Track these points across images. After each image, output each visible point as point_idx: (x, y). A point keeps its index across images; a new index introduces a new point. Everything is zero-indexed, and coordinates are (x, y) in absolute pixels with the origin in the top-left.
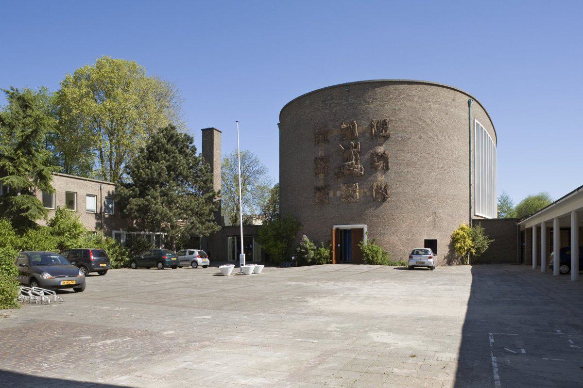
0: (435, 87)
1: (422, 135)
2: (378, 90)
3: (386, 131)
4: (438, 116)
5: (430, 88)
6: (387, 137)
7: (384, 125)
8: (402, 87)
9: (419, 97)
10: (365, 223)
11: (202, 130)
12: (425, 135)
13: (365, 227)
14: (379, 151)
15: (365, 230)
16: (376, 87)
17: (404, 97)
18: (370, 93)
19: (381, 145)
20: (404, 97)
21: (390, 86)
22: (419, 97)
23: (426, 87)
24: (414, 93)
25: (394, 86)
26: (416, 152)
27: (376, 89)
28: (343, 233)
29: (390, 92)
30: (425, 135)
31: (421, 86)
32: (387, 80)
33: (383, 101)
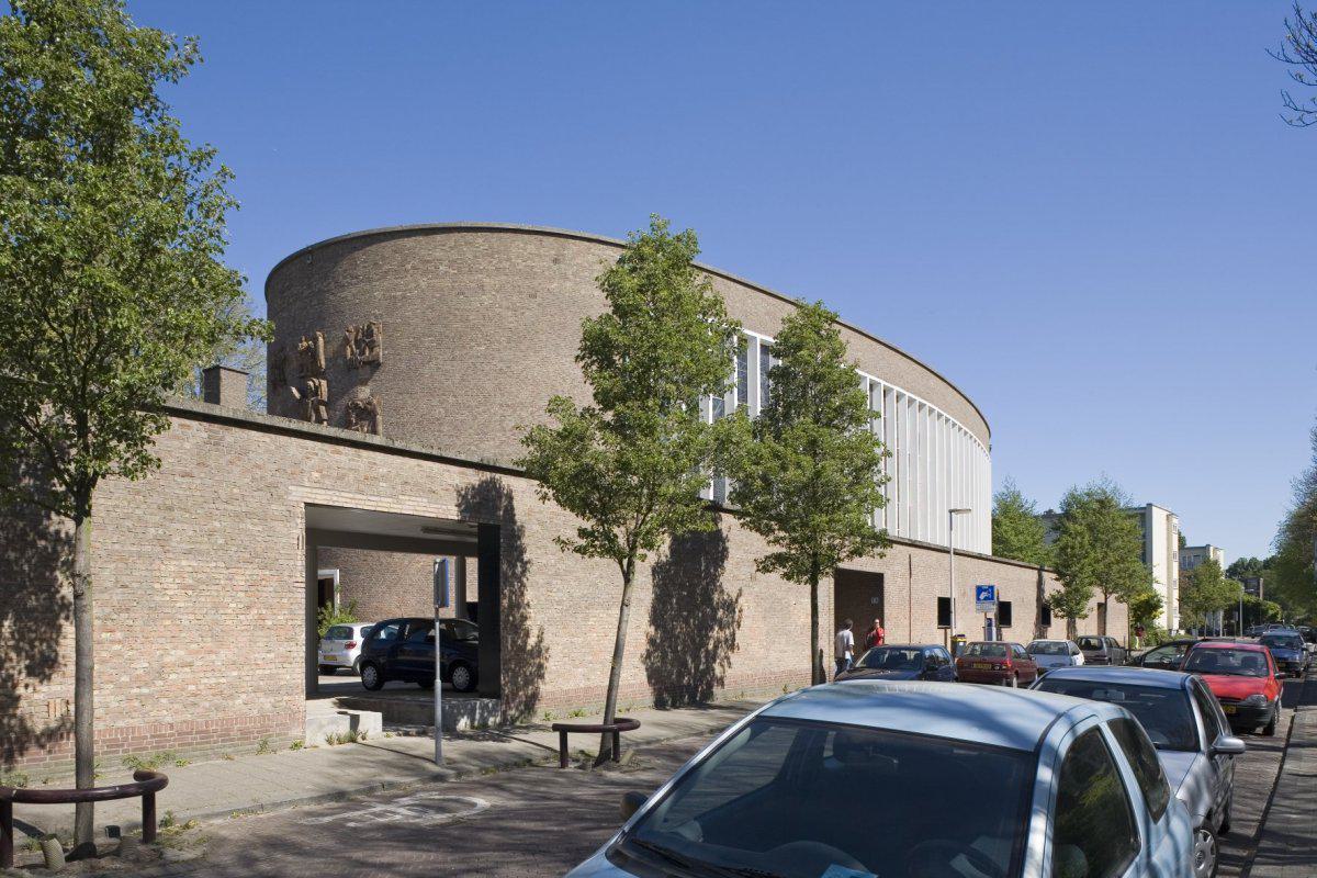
0: (496, 235)
1: (457, 353)
2: (360, 256)
3: (371, 350)
4: (504, 303)
5: (480, 238)
6: (375, 365)
7: (367, 338)
8: (409, 242)
9: (452, 263)
10: (337, 567)
11: (1150, 505)
12: (465, 351)
13: (337, 575)
14: (361, 396)
15: (337, 580)
16: (356, 249)
17: (414, 268)
18: (345, 264)
19: (364, 382)
20: (414, 268)
21: (383, 244)
22: (452, 263)
23: (469, 236)
24: (438, 254)
25: (392, 242)
26: (443, 395)
27: (356, 254)
28: (1229, 851)
29: (383, 258)
30: (465, 351)
31: (456, 236)
32: (375, 232)
33: (369, 280)
